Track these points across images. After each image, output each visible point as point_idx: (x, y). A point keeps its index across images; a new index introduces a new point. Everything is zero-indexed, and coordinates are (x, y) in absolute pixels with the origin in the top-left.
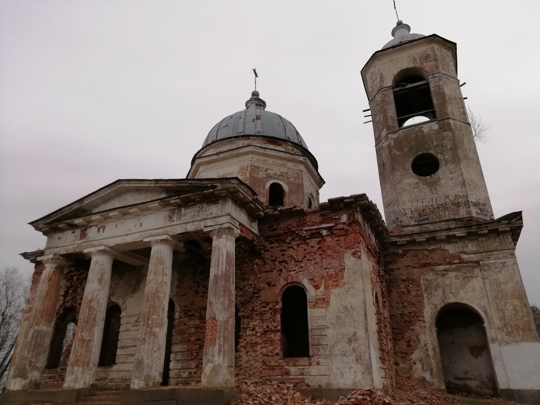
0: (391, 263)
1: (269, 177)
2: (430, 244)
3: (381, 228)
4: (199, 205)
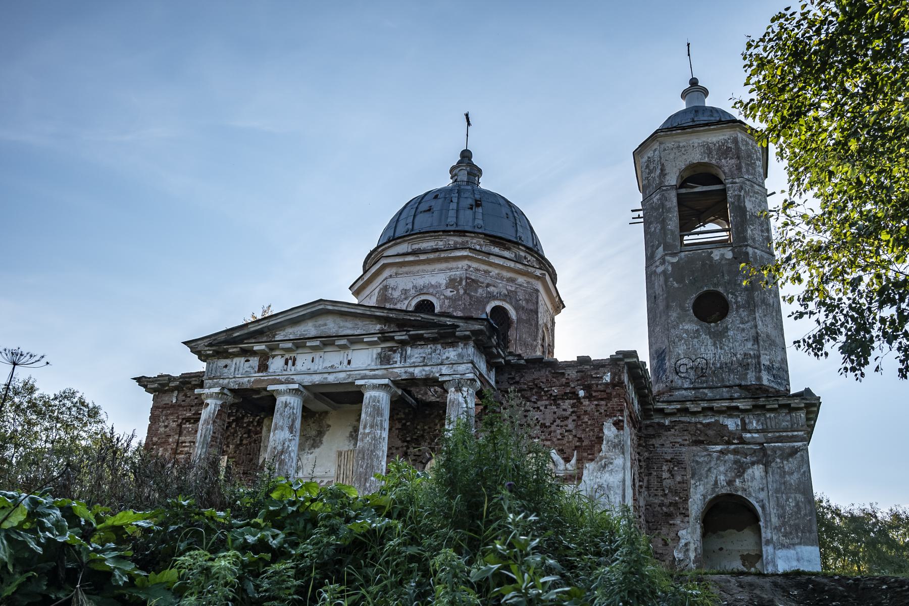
0: (653, 436)
1: (491, 297)
2: (705, 416)
3: (646, 391)
4: (432, 345)
